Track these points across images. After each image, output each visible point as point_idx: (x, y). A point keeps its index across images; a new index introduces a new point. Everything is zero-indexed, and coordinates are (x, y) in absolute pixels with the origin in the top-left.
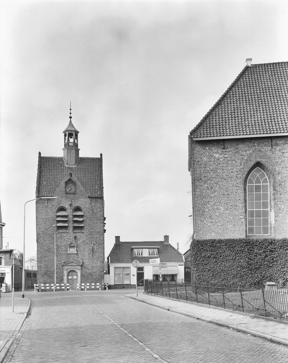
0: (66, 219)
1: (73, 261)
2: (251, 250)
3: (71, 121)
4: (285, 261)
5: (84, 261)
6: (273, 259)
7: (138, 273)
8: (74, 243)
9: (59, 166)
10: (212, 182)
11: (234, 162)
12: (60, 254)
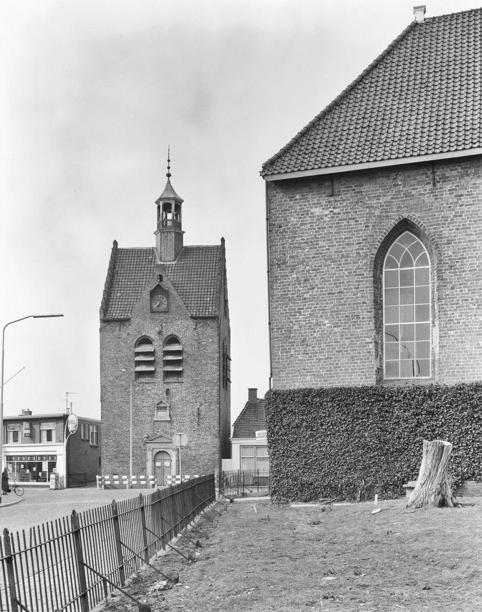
0: (152, 359)
1: (162, 434)
2: (386, 412)
3: (169, 182)
4: (460, 434)
6: (434, 431)
8: (164, 401)
9: (147, 263)
10: (308, 268)
11: (352, 222)
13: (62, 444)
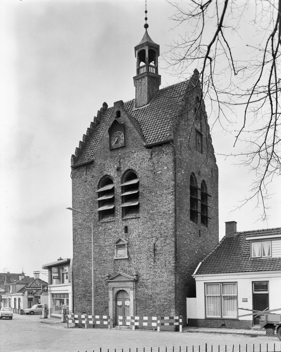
3: (147, 32)
5: (140, 272)
7: (254, 296)
12: (104, 261)
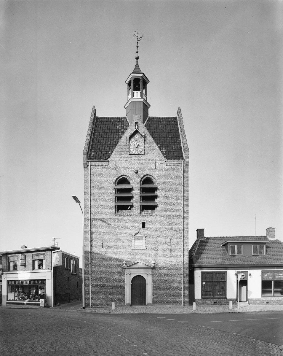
3: (137, 65)
13: (50, 271)
